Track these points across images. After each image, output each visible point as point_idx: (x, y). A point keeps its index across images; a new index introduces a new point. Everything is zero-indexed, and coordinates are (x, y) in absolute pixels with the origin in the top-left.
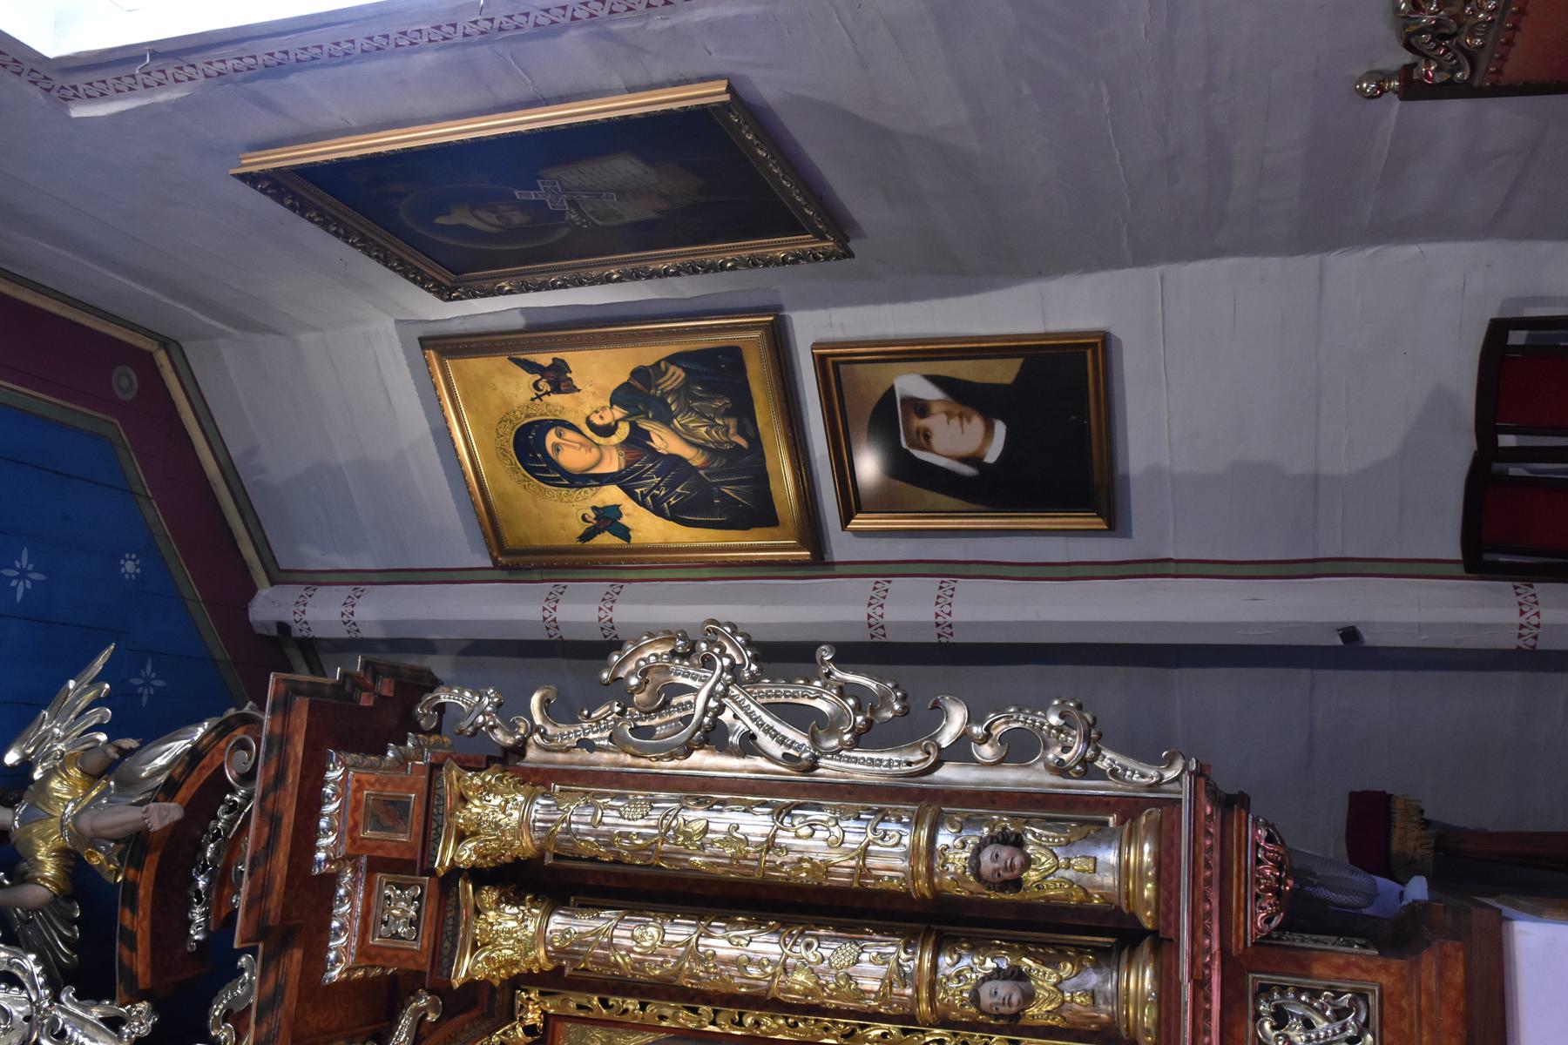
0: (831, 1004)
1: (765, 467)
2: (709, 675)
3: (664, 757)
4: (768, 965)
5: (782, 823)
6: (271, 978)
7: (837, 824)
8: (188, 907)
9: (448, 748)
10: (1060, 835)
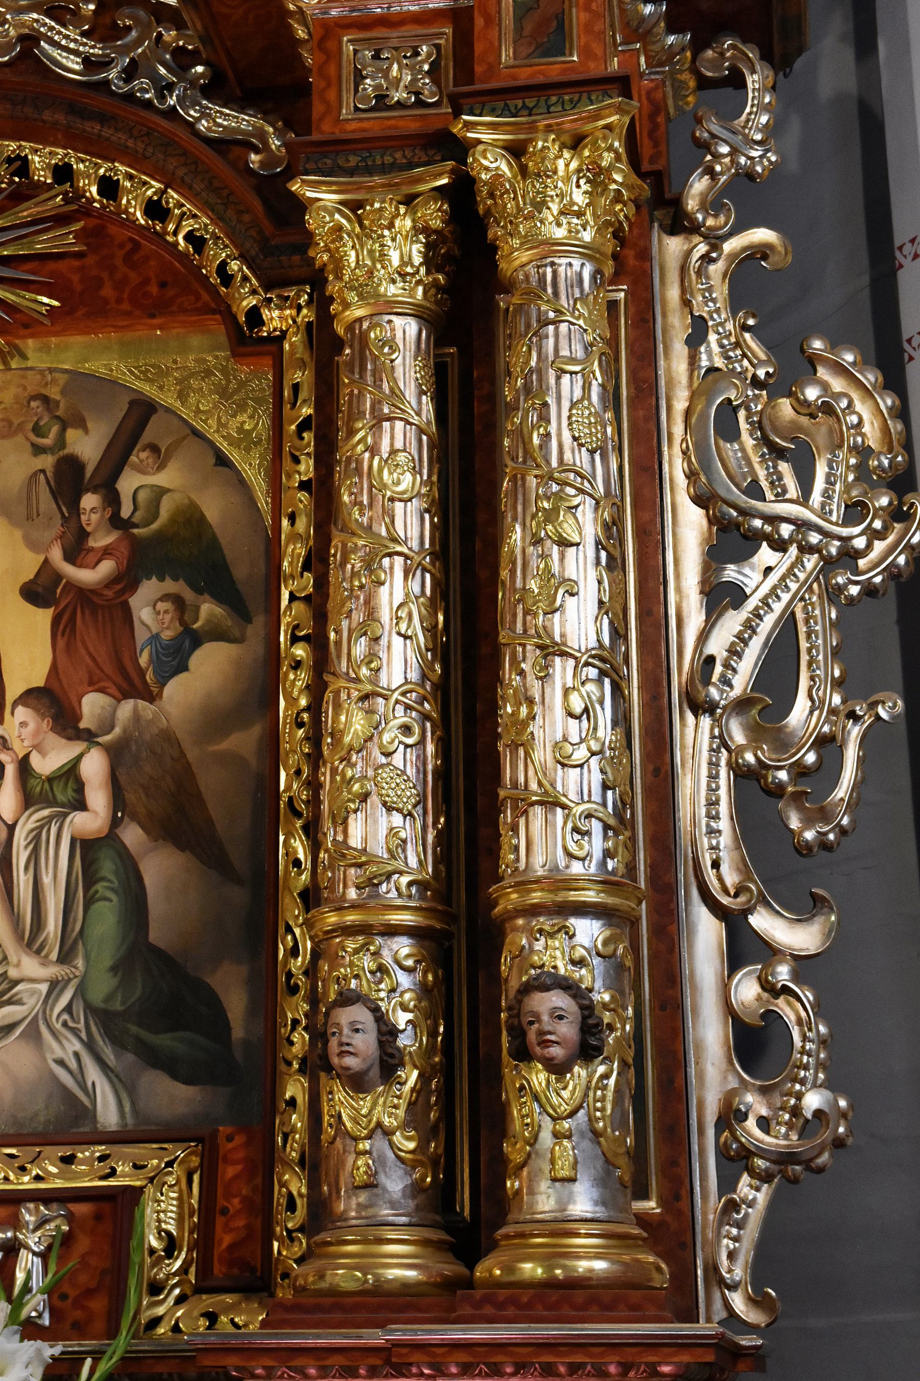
0: (324, 774)
2: (834, 518)
3: (690, 462)
4: (371, 670)
5: (587, 664)
7: (593, 754)
9: (676, 107)
10: (608, 1121)
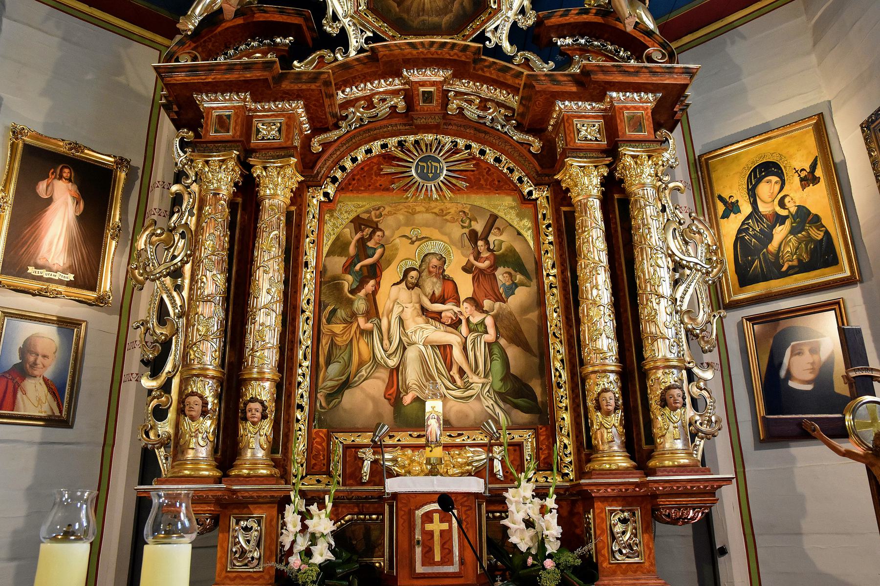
1: (772, 279)
6: (565, 79)
8: (571, 36)
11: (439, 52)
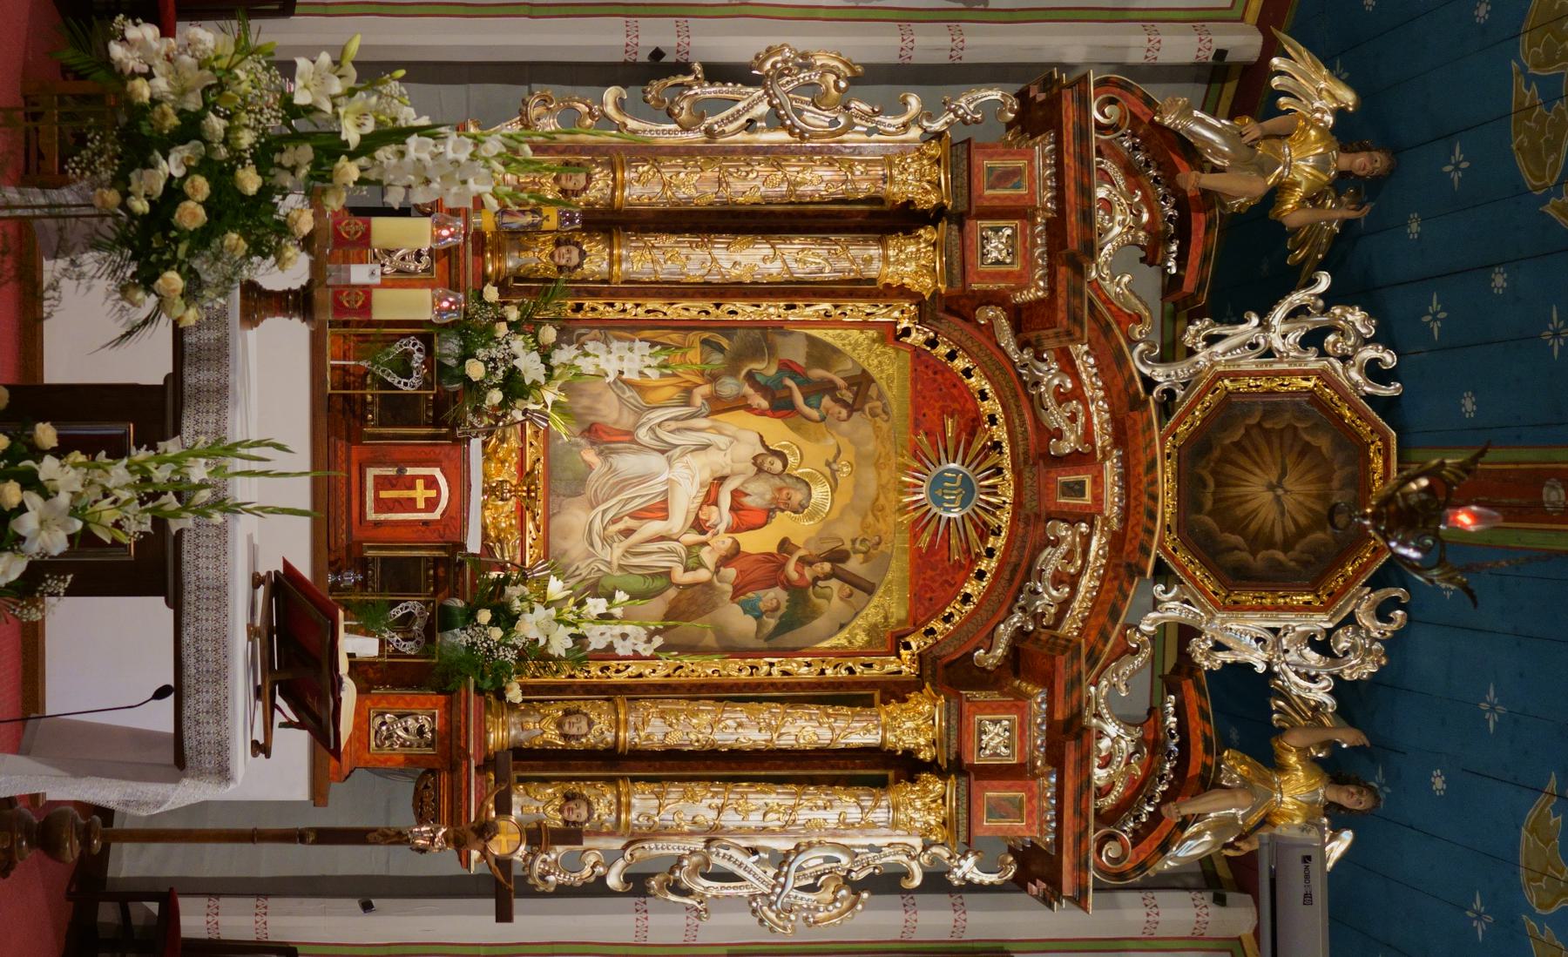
6: (1075, 702)
11: (1142, 509)
